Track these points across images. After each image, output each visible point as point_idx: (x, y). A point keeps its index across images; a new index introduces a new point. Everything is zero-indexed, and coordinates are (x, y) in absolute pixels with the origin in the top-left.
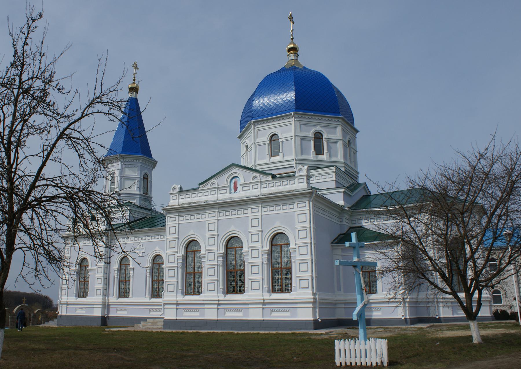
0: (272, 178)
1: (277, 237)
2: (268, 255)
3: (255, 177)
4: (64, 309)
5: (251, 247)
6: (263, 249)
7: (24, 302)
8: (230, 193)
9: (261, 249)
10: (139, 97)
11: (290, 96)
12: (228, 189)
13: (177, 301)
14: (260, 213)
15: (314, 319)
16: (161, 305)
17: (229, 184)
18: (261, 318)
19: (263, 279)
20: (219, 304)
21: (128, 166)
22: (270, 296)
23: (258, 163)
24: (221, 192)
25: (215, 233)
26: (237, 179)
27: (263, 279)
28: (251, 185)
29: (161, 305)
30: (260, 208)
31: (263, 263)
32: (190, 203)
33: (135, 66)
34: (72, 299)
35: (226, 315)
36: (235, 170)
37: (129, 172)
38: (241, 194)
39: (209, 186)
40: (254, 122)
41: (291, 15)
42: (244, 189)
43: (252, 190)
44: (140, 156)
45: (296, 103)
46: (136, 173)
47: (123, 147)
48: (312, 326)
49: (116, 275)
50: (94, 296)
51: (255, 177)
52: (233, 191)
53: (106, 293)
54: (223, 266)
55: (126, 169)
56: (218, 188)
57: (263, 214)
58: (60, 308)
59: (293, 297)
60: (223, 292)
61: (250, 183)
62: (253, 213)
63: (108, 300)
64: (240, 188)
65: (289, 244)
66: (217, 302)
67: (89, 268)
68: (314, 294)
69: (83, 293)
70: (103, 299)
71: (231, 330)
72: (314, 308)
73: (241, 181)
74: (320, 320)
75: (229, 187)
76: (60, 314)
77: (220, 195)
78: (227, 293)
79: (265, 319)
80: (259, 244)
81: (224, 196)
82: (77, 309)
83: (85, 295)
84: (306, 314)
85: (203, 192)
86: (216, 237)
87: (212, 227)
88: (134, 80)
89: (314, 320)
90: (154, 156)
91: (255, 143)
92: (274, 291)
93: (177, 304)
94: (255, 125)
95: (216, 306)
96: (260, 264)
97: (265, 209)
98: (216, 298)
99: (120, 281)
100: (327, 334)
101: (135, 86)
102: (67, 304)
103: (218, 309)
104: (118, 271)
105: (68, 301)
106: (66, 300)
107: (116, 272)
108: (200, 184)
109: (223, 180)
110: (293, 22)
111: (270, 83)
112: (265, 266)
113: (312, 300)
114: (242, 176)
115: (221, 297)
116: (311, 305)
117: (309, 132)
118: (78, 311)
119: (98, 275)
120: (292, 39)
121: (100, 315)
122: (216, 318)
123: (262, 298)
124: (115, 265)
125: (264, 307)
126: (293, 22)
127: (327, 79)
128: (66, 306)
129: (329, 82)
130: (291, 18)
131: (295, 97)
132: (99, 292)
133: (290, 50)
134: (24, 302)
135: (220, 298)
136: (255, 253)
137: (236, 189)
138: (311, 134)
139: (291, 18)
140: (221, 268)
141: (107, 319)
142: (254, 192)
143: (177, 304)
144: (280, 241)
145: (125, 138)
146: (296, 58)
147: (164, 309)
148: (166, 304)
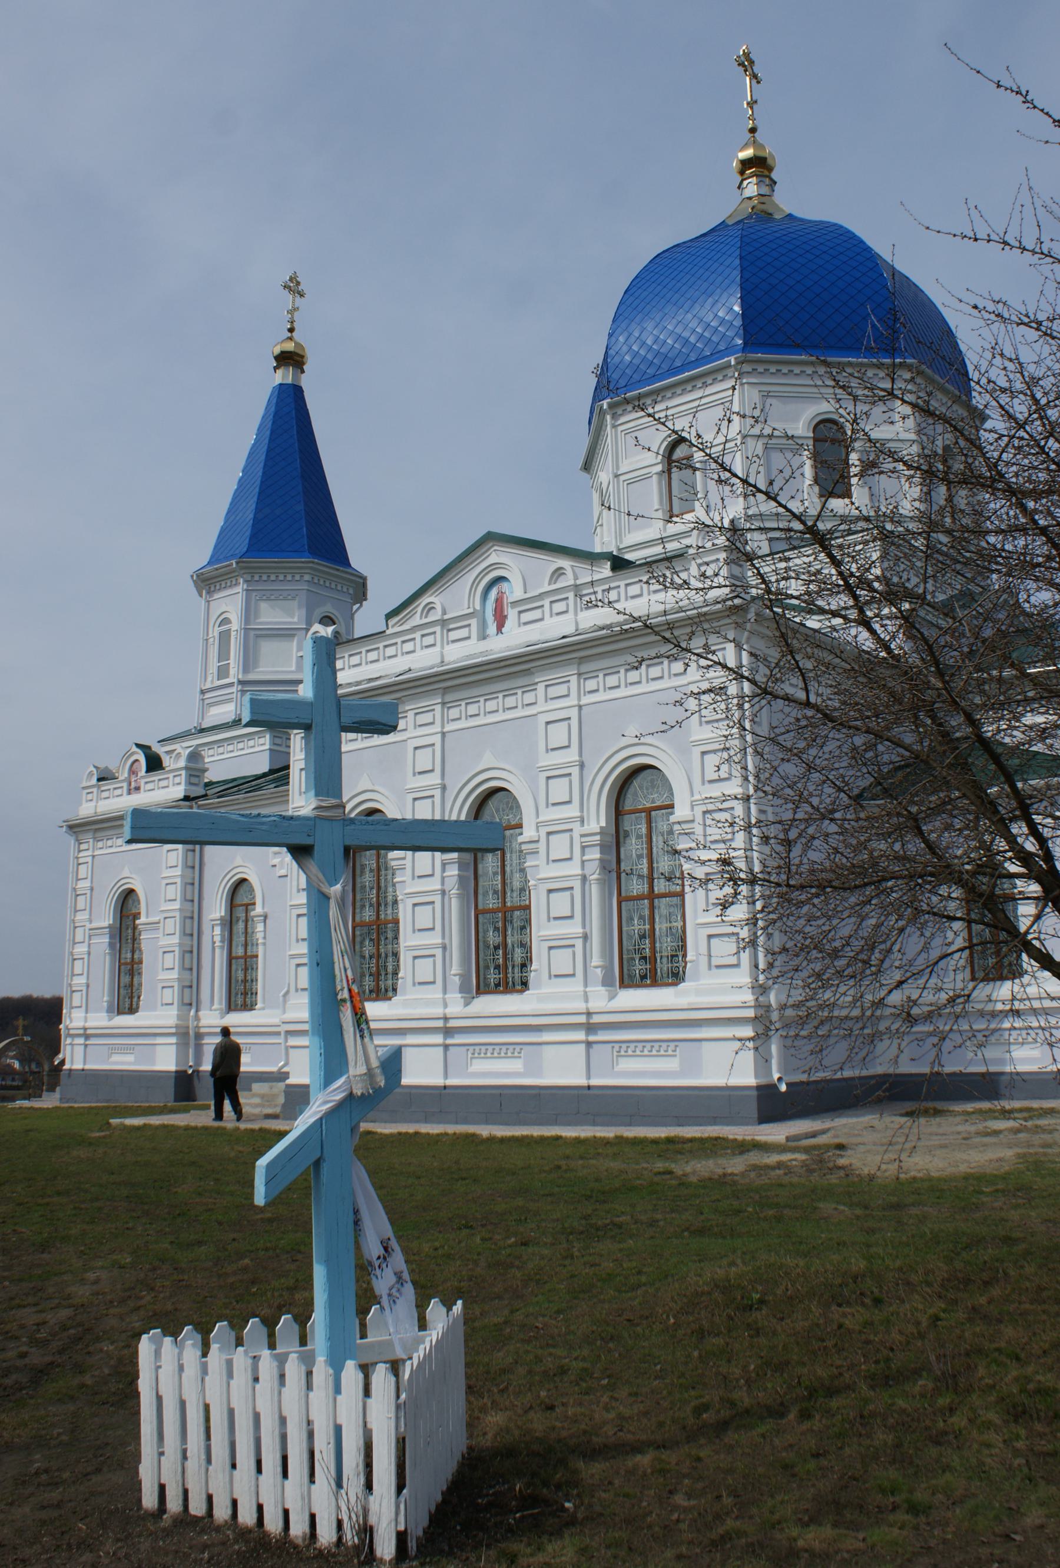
0: (614, 569)
1: (636, 783)
2: (603, 847)
3: (559, 572)
4: (79, 1051)
5: (546, 823)
6: (586, 829)
7: (20, 1031)
8: (483, 636)
9: (578, 830)
10: (306, 382)
11: (731, 307)
12: (474, 622)
13: (589, 1014)
14: (572, 701)
15: (763, 1081)
16: (278, 1034)
17: (478, 607)
18: (582, 1081)
19: (585, 937)
20: (448, 1032)
21: (268, 597)
22: (612, 997)
23: (630, 539)
24: (453, 635)
25: (435, 779)
26: (505, 586)
27: (585, 937)
28: (546, 603)
29: (278, 1034)
30: (574, 680)
31: (584, 878)
32: (358, 683)
33: (293, 286)
34: (99, 1020)
35: (471, 1069)
36: (497, 555)
37: (271, 615)
38: (515, 637)
39: (417, 620)
40: (611, 406)
41: (746, 55)
42: (525, 617)
43: (548, 621)
44: (304, 560)
45: (745, 326)
46: (293, 617)
47: (253, 536)
48: (752, 1109)
49: (217, 939)
50: (154, 1009)
51: (559, 572)
52: (492, 628)
53: (190, 997)
54: (460, 896)
55: (264, 606)
56: (443, 623)
57: (585, 700)
58: (68, 1048)
59: (683, 1001)
60: (464, 989)
61: (541, 596)
62: (553, 699)
63: (197, 1018)
64: (512, 614)
65: (672, 806)
66: (582, 1019)
67: (143, 919)
68: (760, 990)
69: (127, 999)
70: (179, 1017)
71: (465, 1121)
72: (761, 1038)
73: (514, 591)
74: (783, 1088)
75: (480, 615)
76: (66, 1067)
77: (449, 648)
78: (480, 992)
79: (595, 1082)
80: (573, 811)
81: (461, 650)
82: (114, 1049)
83: (132, 1010)
84: (730, 1065)
85: (399, 640)
86: (437, 793)
87: (424, 760)
88: (291, 330)
89: (759, 1088)
90: (357, 560)
91: (617, 476)
92: (627, 981)
93: (590, 1028)
94: (614, 417)
95: (438, 1039)
96: (577, 885)
97: (591, 684)
98: (439, 1011)
99: (231, 959)
100: (791, 1144)
101: (290, 346)
102: (87, 1037)
103: (446, 1047)
104: (222, 925)
105: (88, 1025)
106: (81, 1024)
107: (218, 930)
108: (389, 616)
109: (459, 596)
110: (754, 76)
111: (665, 277)
112: (595, 890)
113: (751, 1013)
114: (521, 572)
115: (456, 1006)
116: (748, 1032)
117: (796, 419)
118: (115, 1058)
119: (165, 941)
120: (753, 130)
121: (172, 1067)
122: (439, 1081)
123: (581, 1006)
124: (216, 909)
125: (591, 1038)
126: (754, 76)
127: (862, 242)
128: (81, 1041)
129: (868, 249)
130: (746, 63)
131: (742, 307)
132: (169, 995)
133: (746, 164)
134: (20, 1031)
135: (451, 1011)
136: (560, 846)
137: (501, 620)
138: (800, 424)
139: (746, 63)
140: (455, 903)
141: (195, 1079)
142: (556, 626)
143: (590, 1028)
144: (640, 796)
145: (258, 510)
146: (765, 190)
147: (287, 1048)
148: (289, 1033)
